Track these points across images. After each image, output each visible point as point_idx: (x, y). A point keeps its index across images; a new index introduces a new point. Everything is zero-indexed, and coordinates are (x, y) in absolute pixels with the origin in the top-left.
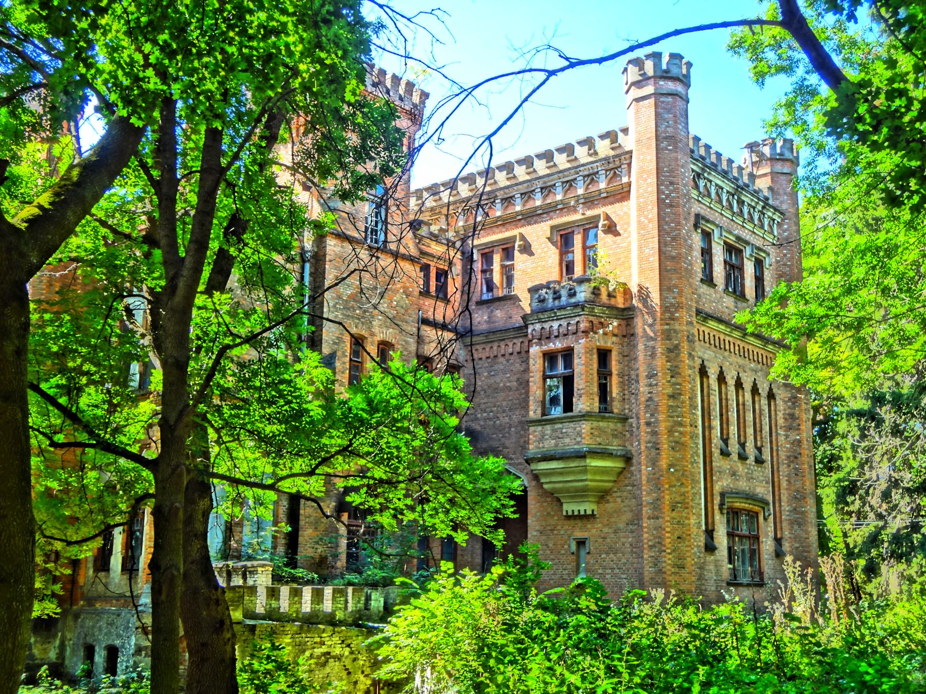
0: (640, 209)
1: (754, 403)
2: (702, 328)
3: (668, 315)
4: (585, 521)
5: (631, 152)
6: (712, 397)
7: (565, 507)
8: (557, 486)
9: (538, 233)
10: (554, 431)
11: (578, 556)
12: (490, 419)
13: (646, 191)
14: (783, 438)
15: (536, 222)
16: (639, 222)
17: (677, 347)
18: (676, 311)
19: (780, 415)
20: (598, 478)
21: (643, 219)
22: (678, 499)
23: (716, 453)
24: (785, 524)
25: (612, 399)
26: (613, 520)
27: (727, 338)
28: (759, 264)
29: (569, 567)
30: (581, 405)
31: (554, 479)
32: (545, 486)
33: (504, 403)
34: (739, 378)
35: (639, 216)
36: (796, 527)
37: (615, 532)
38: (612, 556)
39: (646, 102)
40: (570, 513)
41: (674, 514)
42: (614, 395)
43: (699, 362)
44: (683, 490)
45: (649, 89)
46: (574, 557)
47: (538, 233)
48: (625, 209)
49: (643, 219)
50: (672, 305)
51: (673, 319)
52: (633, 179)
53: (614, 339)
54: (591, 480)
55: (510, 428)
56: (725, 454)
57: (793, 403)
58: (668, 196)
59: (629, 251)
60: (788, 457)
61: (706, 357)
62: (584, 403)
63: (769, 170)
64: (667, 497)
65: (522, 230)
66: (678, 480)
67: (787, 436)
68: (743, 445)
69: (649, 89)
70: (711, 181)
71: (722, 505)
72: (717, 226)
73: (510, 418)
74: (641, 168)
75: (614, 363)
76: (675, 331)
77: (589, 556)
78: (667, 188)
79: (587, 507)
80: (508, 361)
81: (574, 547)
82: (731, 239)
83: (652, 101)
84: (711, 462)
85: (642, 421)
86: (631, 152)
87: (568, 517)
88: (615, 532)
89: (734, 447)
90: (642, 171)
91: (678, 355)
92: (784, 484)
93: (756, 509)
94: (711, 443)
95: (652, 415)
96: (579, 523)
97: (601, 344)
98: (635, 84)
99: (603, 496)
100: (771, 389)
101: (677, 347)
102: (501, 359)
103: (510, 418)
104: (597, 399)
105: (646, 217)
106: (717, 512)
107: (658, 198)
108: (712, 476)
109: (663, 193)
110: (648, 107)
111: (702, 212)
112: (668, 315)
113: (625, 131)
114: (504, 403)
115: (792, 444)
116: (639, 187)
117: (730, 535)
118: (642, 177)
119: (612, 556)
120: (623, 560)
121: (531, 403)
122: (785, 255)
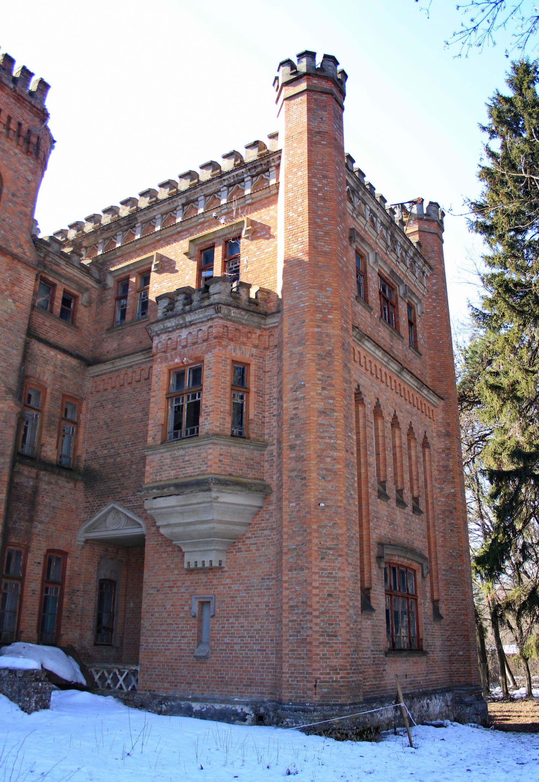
0: (289, 204)
1: (409, 448)
2: (358, 349)
3: (319, 316)
4: (210, 575)
5: (280, 151)
6: (368, 429)
7: (187, 558)
8: (177, 530)
9: (177, 250)
10: (174, 458)
11: (200, 621)
12: (111, 456)
13: (295, 185)
14: (437, 491)
15: (175, 241)
16: (287, 218)
17: (329, 354)
18: (329, 313)
19: (435, 465)
20: (227, 518)
21: (291, 214)
22: (329, 544)
23: (373, 495)
24: (441, 584)
25: (249, 422)
26: (244, 574)
27: (384, 369)
28: (410, 307)
29: (188, 634)
30: (207, 423)
31: (173, 521)
32: (162, 531)
33: (127, 437)
34: (395, 417)
35: (287, 211)
36: (453, 588)
37: (247, 590)
38: (242, 620)
39: (298, 100)
40: (192, 566)
41: (323, 564)
42: (251, 417)
43: (355, 385)
44: (335, 531)
45: (303, 86)
46: (194, 621)
47: (177, 250)
48: (272, 213)
49: (291, 214)
50: (325, 305)
51: (326, 322)
52: (282, 179)
53: (254, 350)
54: (220, 522)
55: (131, 465)
56: (382, 495)
57: (447, 455)
58: (320, 189)
59: (276, 255)
60: (444, 512)
61: (361, 382)
62: (215, 414)
63: (417, 229)
64: (315, 541)
65: (161, 251)
66: (331, 519)
67: (442, 489)
68: (400, 492)
69: (303, 86)
70: (365, 204)
71: (380, 558)
72: (373, 250)
73: (132, 453)
74: (291, 162)
75: (252, 378)
76: (328, 335)
77: (214, 620)
78: (320, 180)
79: (212, 558)
80: (134, 390)
81: (196, 609)
82: (386, 271)
83: (304, 97)
84: (368, 504)
85: (285, 445)
86: (280, 151)
87: (190, 571)
88: (247, 590)
89: (391, 492)
90: (291, 165)
91: (330, 363)
92: (440, 540)
93: (415, 566)
94: (367, 482)
95: (298, 436)
96: (203, 578)
97: (238, 355)
98: (287, 84)
99: (233, 542)
100: (425, 437)
101: (329, 354)
102: (128, 388)
103: (132, 453)
104: (229, 419)
105: (295, 211)
106: (374, 565)
107: (309, 190)
108: (368, 522)
109: (316, 186)
110: (302, 103)
111: (358, 229)
112: (319, 316)
113: (274, 136)
114: (127, 437)
115: (447, 497)
116: (286, 185)
117: (389, 593)
118: (292, 179)
119: (242, 620)
120: (257, 626)
121: (150, 427)
122: (435, 307)
